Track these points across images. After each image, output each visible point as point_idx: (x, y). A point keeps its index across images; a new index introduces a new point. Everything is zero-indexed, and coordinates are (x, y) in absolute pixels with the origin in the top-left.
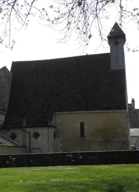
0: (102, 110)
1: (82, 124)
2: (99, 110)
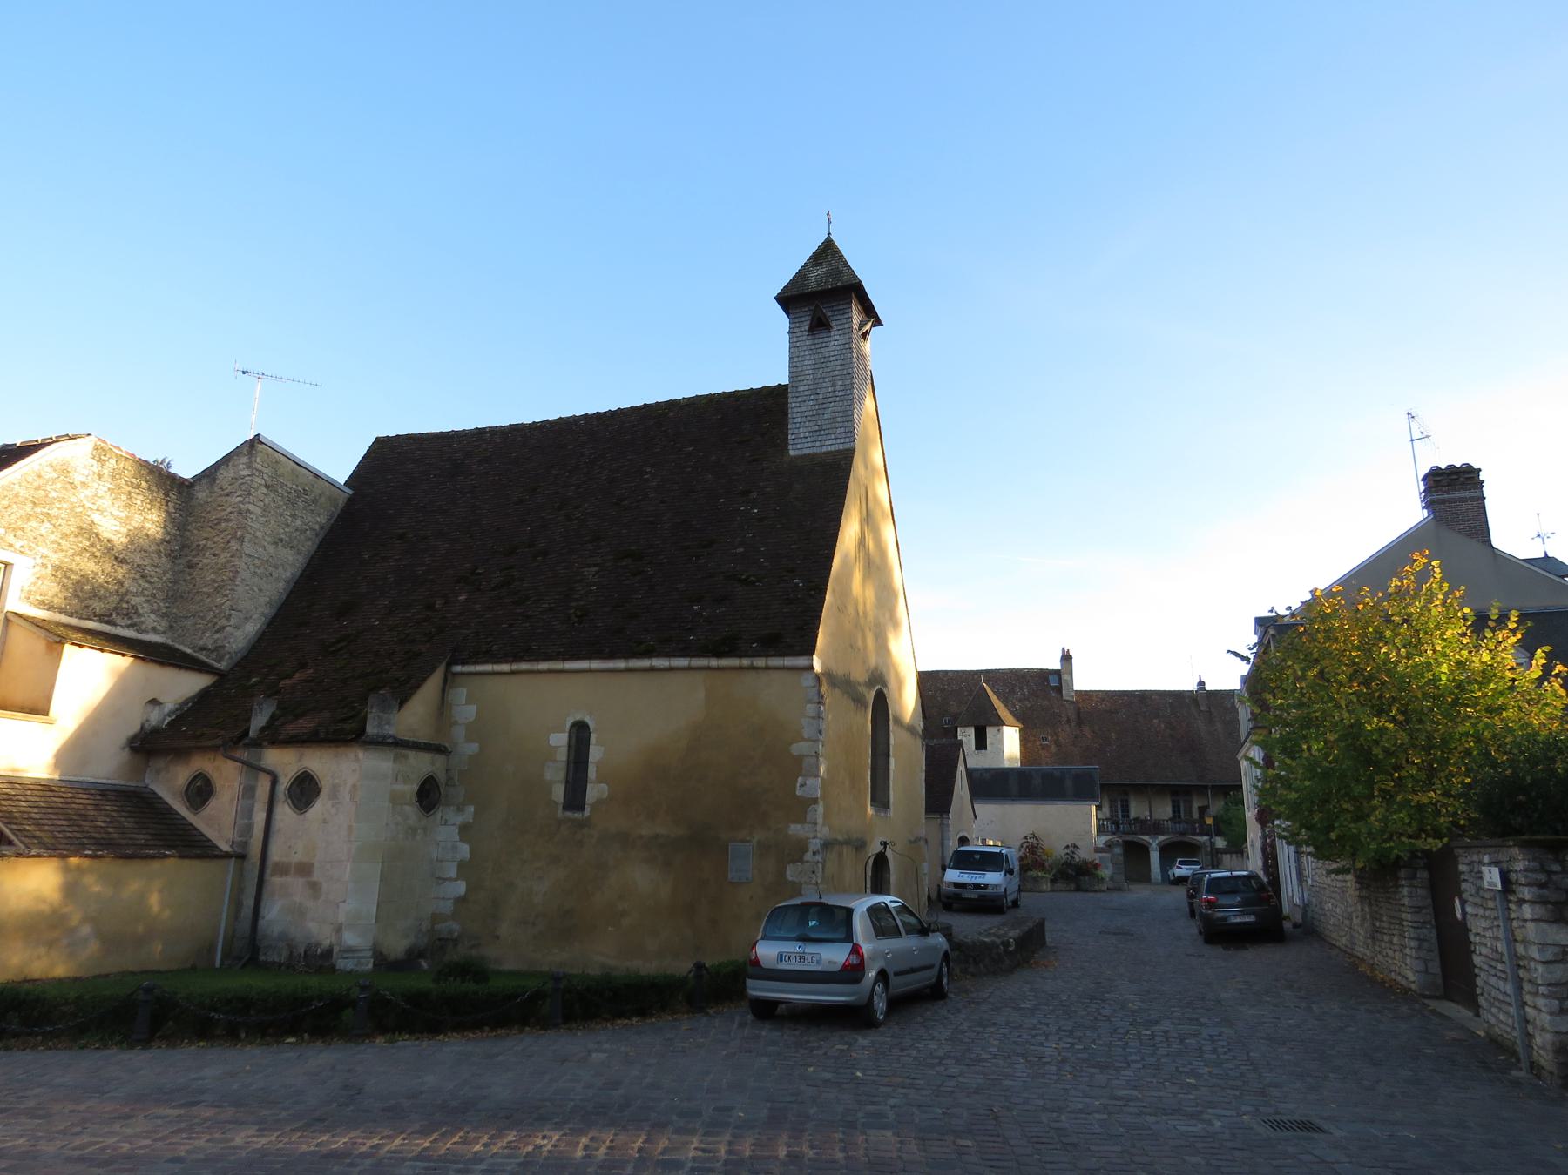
0: (685, 652)
1: (580, 733)
2: (668, 655)
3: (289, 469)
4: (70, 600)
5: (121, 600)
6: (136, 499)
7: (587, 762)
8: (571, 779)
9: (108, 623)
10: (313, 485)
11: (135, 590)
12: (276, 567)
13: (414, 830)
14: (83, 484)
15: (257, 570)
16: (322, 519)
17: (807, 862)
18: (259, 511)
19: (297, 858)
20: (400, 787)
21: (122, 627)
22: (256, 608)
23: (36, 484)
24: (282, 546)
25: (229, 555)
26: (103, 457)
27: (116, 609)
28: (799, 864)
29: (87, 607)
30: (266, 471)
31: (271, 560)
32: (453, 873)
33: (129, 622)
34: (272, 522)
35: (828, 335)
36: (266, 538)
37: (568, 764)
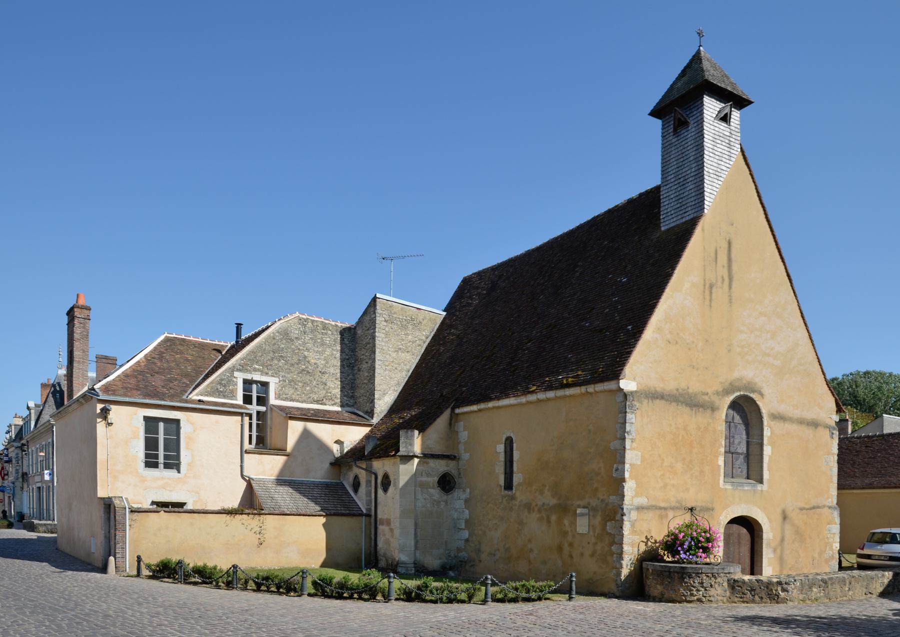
1: (509, 442)
3: (399, 308)
4: (300, 395)
5: (327, 392)
6: (326, 340)
9: (321, 404)
10: (417, 315)
11: (333, 386)
12: (399, 364)
13: (438, 502)
14: (296, 338)
18: (383, 336)
19: (385, 517)
21: (329, 405)
22: (390, 388)
23: (273, 343)
26: (304, 323)
27: (325, 397)
28: (613, 522)
29: (310, 397)
32: (463, 527)
33: (333, 402)
34: (393, 340)
35: (687, 129)
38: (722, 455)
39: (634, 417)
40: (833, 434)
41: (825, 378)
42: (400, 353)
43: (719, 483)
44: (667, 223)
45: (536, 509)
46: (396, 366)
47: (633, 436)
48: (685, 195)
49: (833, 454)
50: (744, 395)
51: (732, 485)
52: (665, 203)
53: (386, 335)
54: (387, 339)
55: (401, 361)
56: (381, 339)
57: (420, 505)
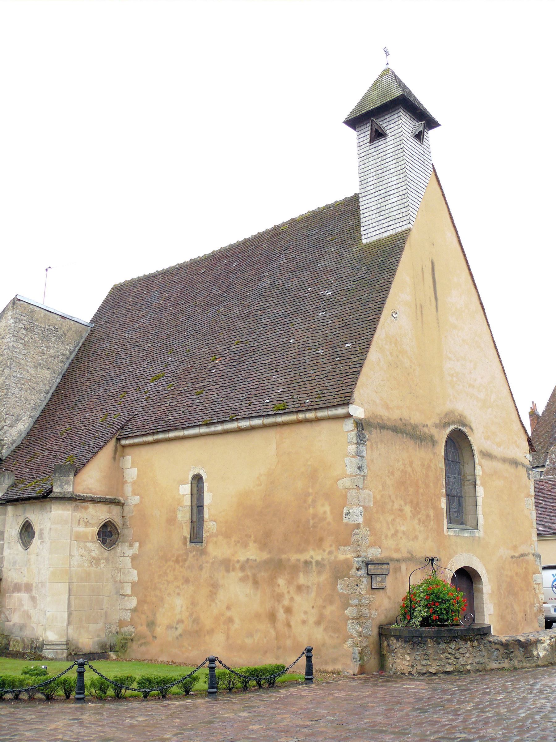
3: (42, 315)
7: (202, 506)
8: (194, 519)
15: (23, 386)
16: (70, 347)
17: (353, 577)
18: (21, 346)
20: (82, 529)
22: (25, 412)
24: (41, 368)
25: (4, 378)
30: (24, 318)
31: (32, 378)
32: (129, 592)
34: (32, 353)
36: (28, 364)
37: (192, 509)
38: (444, 496)
39: (365, 450)
40: (529, 474)
41: (382, 427)
42: (39, 370)
43: (443, 529)
44: (369, 235)
45: (238, 566)
46: (33, 385)
47: (365, 473)
48: (387, 207)
49: (532, 496)
50: (458, 428)
51: (454, 532)
52: (365, 215)
53: (25, 345)
54: (26, 351)
55: (39, 380)
56: (18, 351)
57: (76, 563)
